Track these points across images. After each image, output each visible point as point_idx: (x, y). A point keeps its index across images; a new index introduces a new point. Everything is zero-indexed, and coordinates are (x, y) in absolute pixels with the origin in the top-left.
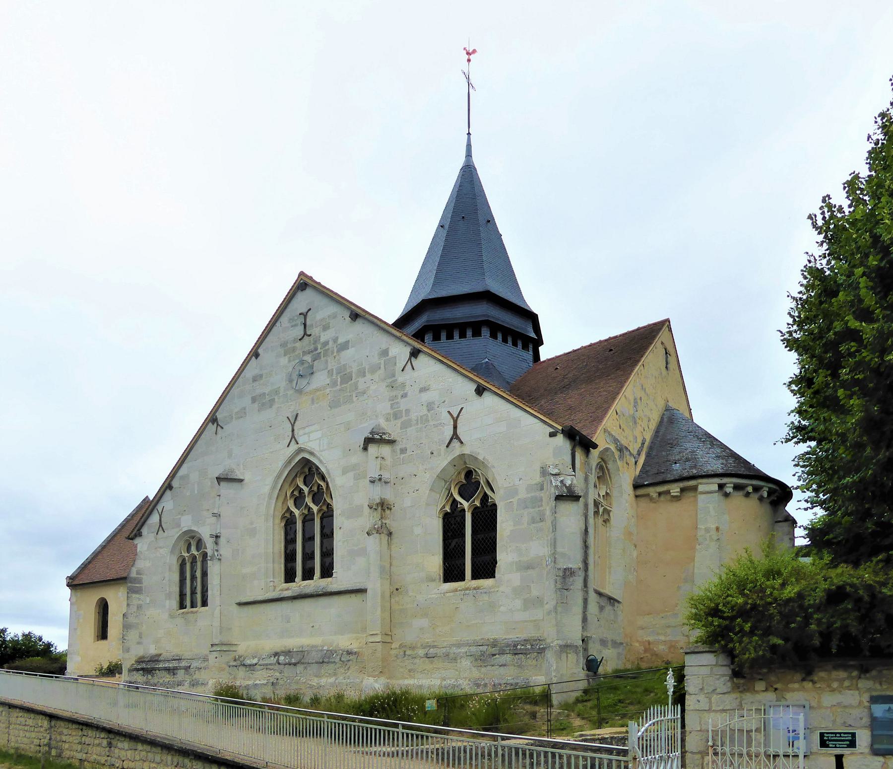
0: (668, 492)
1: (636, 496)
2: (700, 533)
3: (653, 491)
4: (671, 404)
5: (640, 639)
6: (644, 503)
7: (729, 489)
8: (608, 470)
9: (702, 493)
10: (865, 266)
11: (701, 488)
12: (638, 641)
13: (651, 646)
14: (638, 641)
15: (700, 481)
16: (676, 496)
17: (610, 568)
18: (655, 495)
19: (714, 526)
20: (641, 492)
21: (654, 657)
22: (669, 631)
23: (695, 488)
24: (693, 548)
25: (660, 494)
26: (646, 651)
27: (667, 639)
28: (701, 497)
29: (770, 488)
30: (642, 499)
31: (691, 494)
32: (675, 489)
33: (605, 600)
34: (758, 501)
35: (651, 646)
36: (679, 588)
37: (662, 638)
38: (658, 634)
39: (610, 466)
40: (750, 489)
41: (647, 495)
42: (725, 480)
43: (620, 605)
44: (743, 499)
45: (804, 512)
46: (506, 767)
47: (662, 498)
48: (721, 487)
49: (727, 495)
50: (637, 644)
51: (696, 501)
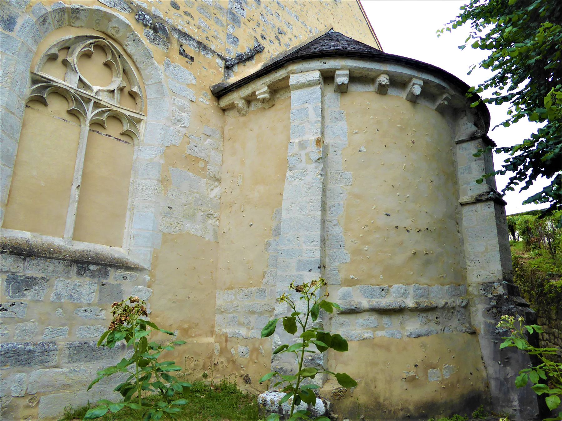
6: (231, 116)
8: (129, 56)
11: (293, 80)
13: (229, 345)
17: (132, 210)
18: (240, 103)
20: (225, 102)
21: (230, 366)
28: (295, 95)
29: (426, 82)
32: (261, 88)
34: (408, 104)
36: (268, 244)
37: (243, 332)
38: (241, 324)
39: (130, 49)
41: (232, 106)
42: (331, 64)
44: (376, 98)
45: (512, 130)
48: (328, 77)
49: (342, 90)
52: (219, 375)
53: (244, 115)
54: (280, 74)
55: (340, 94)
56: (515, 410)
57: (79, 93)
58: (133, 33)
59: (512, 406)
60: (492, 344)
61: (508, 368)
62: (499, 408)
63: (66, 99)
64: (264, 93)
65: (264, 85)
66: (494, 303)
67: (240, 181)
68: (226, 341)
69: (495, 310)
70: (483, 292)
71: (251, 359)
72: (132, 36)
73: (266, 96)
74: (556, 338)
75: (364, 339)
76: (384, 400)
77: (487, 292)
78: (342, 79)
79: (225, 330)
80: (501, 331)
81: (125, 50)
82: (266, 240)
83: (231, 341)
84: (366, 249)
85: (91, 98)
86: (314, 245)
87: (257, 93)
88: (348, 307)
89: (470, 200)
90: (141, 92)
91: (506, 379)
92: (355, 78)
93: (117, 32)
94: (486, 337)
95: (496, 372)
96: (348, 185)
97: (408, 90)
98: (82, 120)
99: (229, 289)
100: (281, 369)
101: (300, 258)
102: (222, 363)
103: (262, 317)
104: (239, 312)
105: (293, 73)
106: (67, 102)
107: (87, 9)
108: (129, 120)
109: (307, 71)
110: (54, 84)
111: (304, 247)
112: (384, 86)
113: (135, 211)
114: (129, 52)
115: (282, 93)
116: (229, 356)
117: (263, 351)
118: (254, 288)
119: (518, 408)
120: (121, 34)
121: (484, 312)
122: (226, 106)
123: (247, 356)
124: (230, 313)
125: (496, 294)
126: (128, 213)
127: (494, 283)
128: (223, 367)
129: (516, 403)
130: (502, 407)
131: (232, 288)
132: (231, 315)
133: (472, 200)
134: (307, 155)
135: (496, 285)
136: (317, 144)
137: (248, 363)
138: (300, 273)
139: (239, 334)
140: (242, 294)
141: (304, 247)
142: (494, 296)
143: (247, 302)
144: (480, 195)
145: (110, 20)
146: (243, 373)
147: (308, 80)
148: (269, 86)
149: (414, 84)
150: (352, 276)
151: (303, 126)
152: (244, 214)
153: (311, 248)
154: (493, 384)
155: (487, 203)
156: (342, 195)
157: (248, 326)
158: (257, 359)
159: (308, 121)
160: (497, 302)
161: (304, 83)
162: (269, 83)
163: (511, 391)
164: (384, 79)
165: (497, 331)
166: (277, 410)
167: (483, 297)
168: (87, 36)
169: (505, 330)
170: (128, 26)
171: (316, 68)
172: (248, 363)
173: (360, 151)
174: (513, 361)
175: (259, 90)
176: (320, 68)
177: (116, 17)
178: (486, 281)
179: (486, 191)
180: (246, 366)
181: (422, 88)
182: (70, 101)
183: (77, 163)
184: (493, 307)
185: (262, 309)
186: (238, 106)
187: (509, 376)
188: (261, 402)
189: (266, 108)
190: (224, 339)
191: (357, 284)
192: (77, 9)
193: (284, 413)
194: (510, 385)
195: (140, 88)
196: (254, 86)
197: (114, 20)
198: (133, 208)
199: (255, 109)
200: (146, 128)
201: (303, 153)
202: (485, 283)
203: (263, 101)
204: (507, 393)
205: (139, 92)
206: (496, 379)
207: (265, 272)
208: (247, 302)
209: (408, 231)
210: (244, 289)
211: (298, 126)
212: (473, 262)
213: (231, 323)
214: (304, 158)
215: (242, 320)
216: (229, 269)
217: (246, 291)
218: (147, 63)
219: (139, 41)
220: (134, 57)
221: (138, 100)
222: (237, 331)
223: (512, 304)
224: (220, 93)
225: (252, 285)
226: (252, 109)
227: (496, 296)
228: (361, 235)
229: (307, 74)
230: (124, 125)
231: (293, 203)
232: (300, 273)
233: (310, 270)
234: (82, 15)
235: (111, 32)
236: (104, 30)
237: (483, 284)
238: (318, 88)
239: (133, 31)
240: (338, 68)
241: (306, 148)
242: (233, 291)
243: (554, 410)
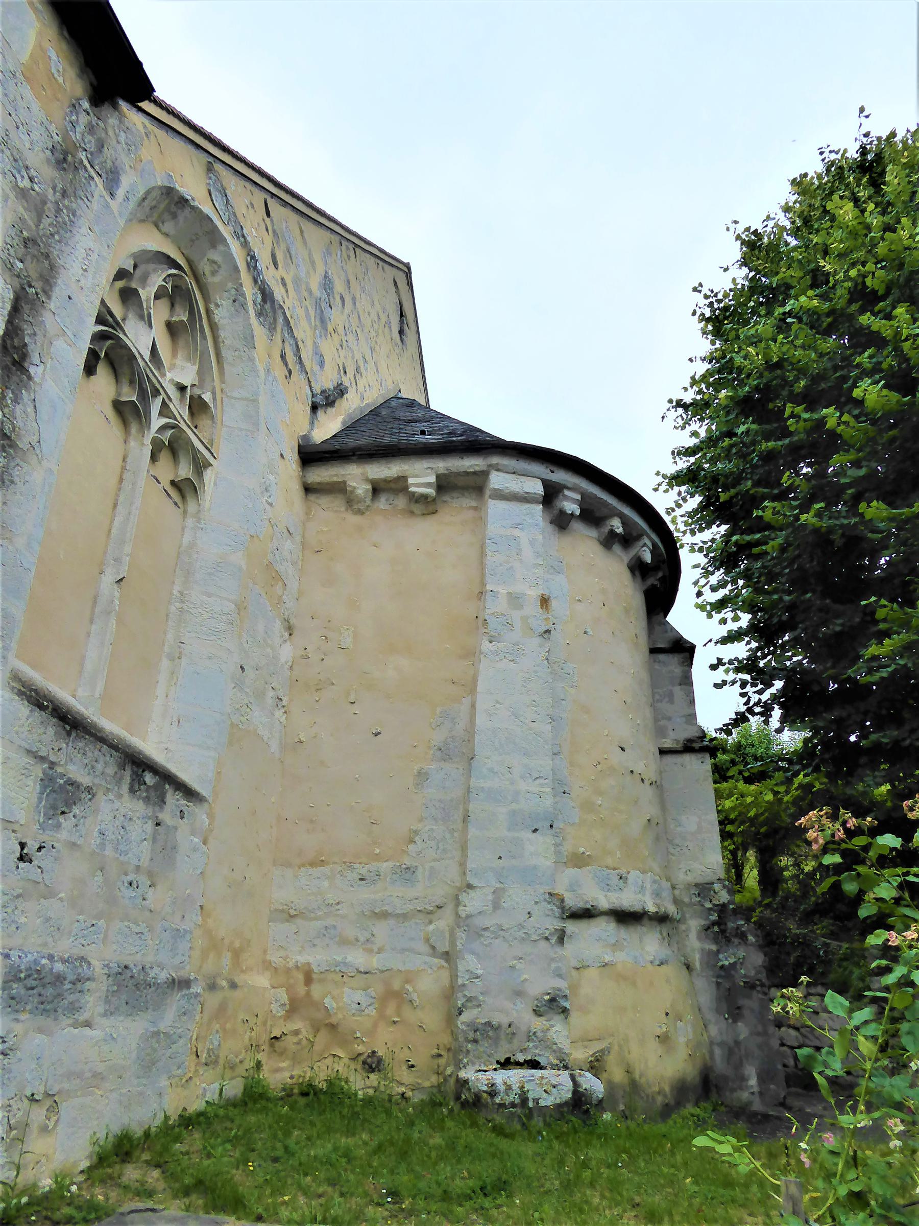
1: (308, 489)
2: (496, 606)
3: (358, 476)
5: (275, 958)
6: (328, 510)
8: (213, 327)
9: (500, 495)
11: (497, 480)
12: (267, 965)
13: (316, 991)
14: (267, 965)
15: (495, 460)
16: (423, 498)
17: (176, 658)
18: (362, 489)
19: (534, 593)
20: (321, 474)
21: (322, 1038)
22: (381, 930)
23: (475, 485)
24: (471, 654)
25: (377, 489)
26: (293, 1008)
27: (375, 962)
28: (495, 508)
30: (324, 501)
31: (468, 501)
32: (421, 475)
33: (107, 764)
35: (316, 991)
37: (357, 958)
38: (344, 942)
39: (222, 315)
41: (338, 489)
42: (561, 476)
43: (200, 814)
47: (382, 503)
48: (551, 494)
49: (561, 522)
50: (262, 981)
51: (480, 521)
52: (284, 1065)
53: (360, 512)
55: (557, 529)
56: (753, 1093)
57: (148, 370)
58: (239, 288)
59: (747, 1087)
60: (714, 985)
61: (739, 1024)
62: (728, 1094)
64: (428, 485)
65: (429, 471)
66: (714, 917)
67: (348, 642)
68: (308, 980)
69: (716, 929)
70: (698, 899)
71: (382, 1015)
72: (233, 292)
73: (431, 491)
75: (606, 964)
76: (641, 1076)
77: (704, 898)
79: (302, 959)
80: (727, 963)
81: (208, 311)
82: (416, 768)
83: (321, 981)
84: (600, 802)
85: (161, 390)
86: (541, 785)
88: (581, 905)
89: (675, 746)
90: (215, 407)
91: (737, 1043)
92: (377, 489)
93: (214, 273)
94: (704, 974)
95: (721, 1034)
96: (572, 686)
97: (633, 552)
98: (134, 428)
99: (312, 864)
100: (489, 1024)
101: (514, 806)
102: (296, 1033)
103: (406, 924)
104: (343, 917)
105: (498, 470)
106: (113, 381)
107: (198, 208)
109: (523, 475)
110: (121, 336)
111: (523, 786)
113: (184, 660)
114: (217, 319)
115: (455, 494)
116: (319, 1015)
117: (415, 996)
118: (385, 865)
119: (756, 1089)
120: (216, 279)
121: (699, 933)
122: (319, 483)
123: (372, 1011)
124: (317, 919)
125: (717, 903)
126: (165, 663)
127: (713, 883)
128: (298, 1043)
129: (753, 1082)
130: (733, 1090)
131: (322, 863)
132: (318, 924)
133: (679, 746)
134: (524, 619)
135: (717, 887)
136: (542, 606)
137: (375, 1025)
138: (516, 835)
139: (345, 964)
140: (353, 876)
141: (523, 786)
142: (714, 905)
143: (365, 895)
144: (690, 741)
145: (214, 246)
146: (361, 1048)
148: (438, 477)
150: (582, 850)
151: (512, 567)
152: (355, 709)
153: (537, 790)
154: (718, 1052)
155: (700, 756)
156: (563, 702)
157: (368, 945)
158: (399, 1016)
159: (521, 561)
160: (719, 916)
162: (442, 471)
163: (744, 1061)
164: (617, 525)
165: (720, 964)
166: (517, 1101)
167: (698, 908)
168: (169, 257)
169: (732, 961)
170: (236, 269)
171: (537, 474)
172: (375, 1025)
173: (585, 633)
174: (746, 1012)
175: (417, 476)
176: (544, 477)
177: (227, 245)
178: (700, 880)
179: (697, 735)
180: (371, 1033)
183: (116, 523)
184: (714, 924)
185: (410, 907)
186: (352, 492)
187: (742, 1037)
188: (485, 1088)
189: (417, 512)
190: (301, 977)
191: (587, 865)
192: (187, 200)
193: (531, 1104)
194: (743, 1052)
195: (214, 399)
197: (221, 248)
198: (181, 653)
199: (388, 507)
200: (215, 484)
201: (516, 615)
202: (701, 884)
204: (739, 1066)
205: (212, 405)
206: (722, 1044)
207: (416, 832)
208: (365, 895)
209: (642, 780)
210: (356, 866)
211: (501, 565)
212: (679, 849)
213: (317, 941)
214: (518, 624)
215: (351, 932)
216: (312, 821)
217: (364, 871)
218: (243, 354)
219: (243, 306)
220: (222, 334)
222: (339, 958)
223: (742, 919)
224: (311, 456)
225: (377, 858)
226: (382, 507)
227: (718, 905)
228: (593, 778)
229: (523, 479)
230: (181, 465)
231: (498, 702)
232: (516, 835)
233: (535, 830)
234: (184, 215)
235: (204, 267)
236: (194, 257)
237: (697, 885)
239: (241, 285)
240: (569, 485)
241: (521, 607)
242: (326, 870)
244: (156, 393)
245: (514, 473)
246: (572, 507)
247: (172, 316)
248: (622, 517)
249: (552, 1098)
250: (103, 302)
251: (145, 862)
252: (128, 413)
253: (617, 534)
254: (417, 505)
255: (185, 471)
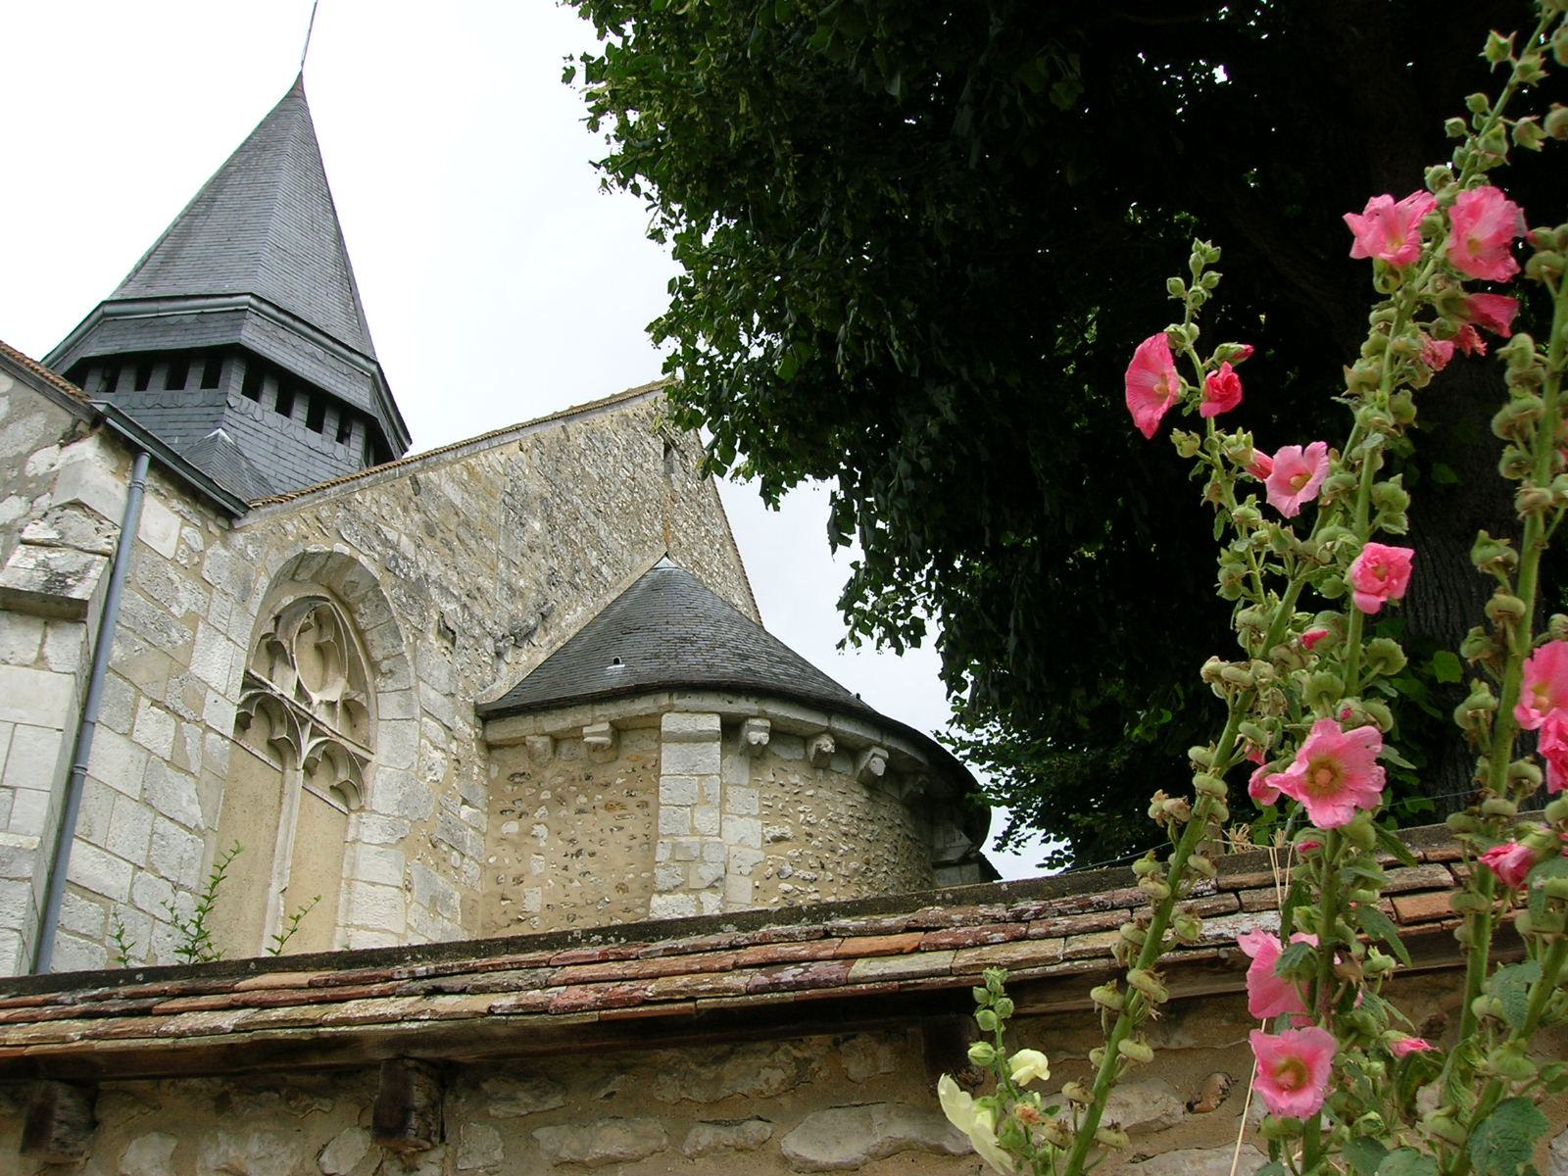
0: (575, 735)
1: (490, 747)
3: (533, 730)
4: (1510, 361)
7: (758, 736)
8: (360, 633)
10: (1437, 811)
11: (670, 723)
18: (540, 743)
20: (499, 732)
23: (650, 724)
25: (556, 740)
32: (596, 727)
40: (827, 744)
46: (1, 1015)
48: (731, 728)
49: (756, 756)
54: (642, 706)
57: (294, 708)
63: (269, 718)
73: (606, 739)
74: (658, 151)
78: (757, 735)
87: (586, 730)
92: (556, 740)
108: (351, 761)
109: (697, 712)
112: (826, 754)
147: (699, 728)
149: (874, 755)
161: (692, 733)
181: (887, 762)
182: (276, 721)
183: (280, 838)
196: (580, 717)
203: (597, 748)
221: (362, 721)
224: (488, 715)
238: (716, 747)
243: (984, 1071)
244: (304, 722)
245: (687, 711)
246: (758, 736)
247: (321, 637)
248: (829, 731)
249: (211, 1166)
250: (247, 672)
251: (1272, 919)
252: (282, 750)
253: (826, 753)
254: (596, 754)
255: (343, 775)
